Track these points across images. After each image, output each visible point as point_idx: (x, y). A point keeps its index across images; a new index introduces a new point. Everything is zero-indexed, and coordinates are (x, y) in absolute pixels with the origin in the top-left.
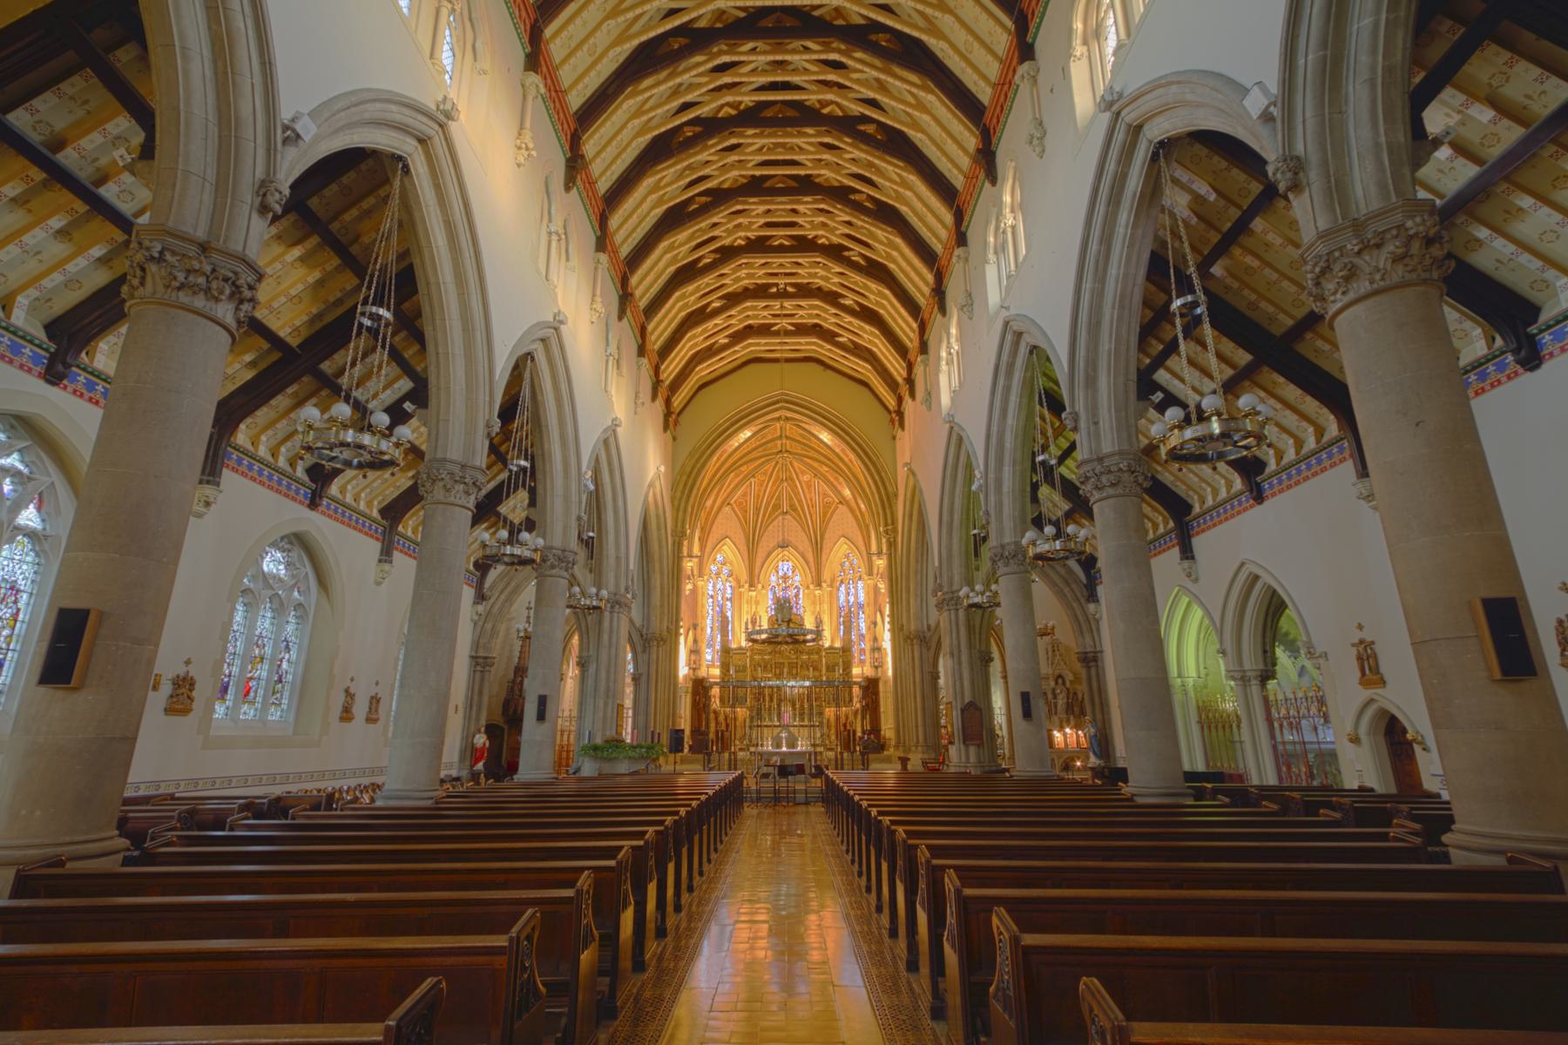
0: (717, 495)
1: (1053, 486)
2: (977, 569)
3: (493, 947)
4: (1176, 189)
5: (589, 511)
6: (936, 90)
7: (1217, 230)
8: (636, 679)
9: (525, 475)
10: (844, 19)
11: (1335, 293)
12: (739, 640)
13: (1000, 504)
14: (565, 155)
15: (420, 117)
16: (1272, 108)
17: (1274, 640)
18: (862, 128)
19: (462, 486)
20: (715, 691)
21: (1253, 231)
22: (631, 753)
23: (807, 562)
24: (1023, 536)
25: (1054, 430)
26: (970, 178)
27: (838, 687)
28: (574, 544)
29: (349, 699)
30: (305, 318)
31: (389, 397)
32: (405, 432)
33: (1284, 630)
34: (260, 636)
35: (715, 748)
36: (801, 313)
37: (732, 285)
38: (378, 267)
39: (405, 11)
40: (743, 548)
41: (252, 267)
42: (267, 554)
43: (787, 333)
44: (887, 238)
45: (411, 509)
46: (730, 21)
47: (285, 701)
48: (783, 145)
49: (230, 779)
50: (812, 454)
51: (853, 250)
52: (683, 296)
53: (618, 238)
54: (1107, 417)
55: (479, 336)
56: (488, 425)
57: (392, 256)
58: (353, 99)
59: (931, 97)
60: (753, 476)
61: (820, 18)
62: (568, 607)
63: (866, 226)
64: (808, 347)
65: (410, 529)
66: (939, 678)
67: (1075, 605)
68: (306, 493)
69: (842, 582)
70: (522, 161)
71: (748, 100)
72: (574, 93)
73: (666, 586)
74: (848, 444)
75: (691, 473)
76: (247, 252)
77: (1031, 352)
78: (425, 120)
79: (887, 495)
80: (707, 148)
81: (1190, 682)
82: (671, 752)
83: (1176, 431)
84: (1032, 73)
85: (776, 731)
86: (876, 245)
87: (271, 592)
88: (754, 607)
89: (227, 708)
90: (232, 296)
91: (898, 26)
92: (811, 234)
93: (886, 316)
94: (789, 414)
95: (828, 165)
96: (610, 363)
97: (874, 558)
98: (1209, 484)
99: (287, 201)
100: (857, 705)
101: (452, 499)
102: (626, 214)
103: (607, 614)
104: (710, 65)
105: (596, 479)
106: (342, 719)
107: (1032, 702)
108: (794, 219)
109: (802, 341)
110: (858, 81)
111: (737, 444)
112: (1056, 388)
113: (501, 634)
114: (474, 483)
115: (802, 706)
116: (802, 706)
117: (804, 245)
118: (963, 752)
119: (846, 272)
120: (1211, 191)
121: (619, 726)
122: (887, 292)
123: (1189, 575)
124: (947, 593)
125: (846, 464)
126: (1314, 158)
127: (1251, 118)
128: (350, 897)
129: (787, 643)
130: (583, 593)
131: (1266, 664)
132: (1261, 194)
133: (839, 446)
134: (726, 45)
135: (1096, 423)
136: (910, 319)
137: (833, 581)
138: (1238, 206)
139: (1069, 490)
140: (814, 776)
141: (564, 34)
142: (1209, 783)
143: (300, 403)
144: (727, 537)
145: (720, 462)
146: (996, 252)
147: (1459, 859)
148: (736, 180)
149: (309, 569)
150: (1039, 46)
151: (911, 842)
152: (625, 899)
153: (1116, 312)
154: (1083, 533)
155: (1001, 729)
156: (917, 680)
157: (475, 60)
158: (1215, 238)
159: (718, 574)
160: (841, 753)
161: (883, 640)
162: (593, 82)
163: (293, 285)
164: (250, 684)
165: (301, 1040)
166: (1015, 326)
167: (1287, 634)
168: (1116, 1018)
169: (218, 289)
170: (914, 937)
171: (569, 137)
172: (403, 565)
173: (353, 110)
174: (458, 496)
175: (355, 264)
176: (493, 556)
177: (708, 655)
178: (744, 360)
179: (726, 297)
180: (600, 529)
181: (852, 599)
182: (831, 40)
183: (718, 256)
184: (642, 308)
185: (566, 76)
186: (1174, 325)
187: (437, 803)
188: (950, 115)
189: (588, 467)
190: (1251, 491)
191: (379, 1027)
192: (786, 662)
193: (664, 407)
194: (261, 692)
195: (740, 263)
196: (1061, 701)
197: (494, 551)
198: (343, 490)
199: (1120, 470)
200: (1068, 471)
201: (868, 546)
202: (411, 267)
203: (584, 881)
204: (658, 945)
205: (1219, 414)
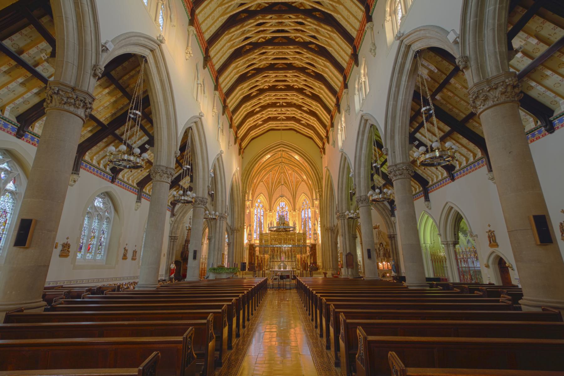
0: (258, 178)
1: (379, 175)
2: (352, 205)
4: (423, 68)
5: (212, 184)
7: (438, 83)
8: (229, 244)
9: (189, 171)
10: (304, 7)
11: (480, 105)
12: (266, 230)
14: (203, 56)
16: (457, 39)
18: (310, 46)
19: (166, 175)
20: (257, 249)
21: (451, 83)
22: (227, 271)
24: (368, 193)
26: (349, 64)
27: (301, 247)
28: (206, 196)
29: (125, 252)
30: (110, 114)
31: (140, 143)
32: (146, 155)
33: (462, 227)
34: (94, 229)
35: (257, 269)
36: (288, 112)
37: (263, 103)
38: (136, 96)
40: (267, 197)
42: (96, 199)
43: (283, 120)
46: (262, 8)
47: (102, 252)
48: (282, 52)
49: (83, 280)
50: (292, 163)
51: (307, 90)
52: (246, 107)
53: (222, 86)
54: (398, 150)
56: (176, 153)
57: (141, 92)
58: (127, 36)
59: (335, 35)
60: (271, 171)
61: (295, 7)
62: (204, 218)
64: (291, 125)
65: (147, 190)
66: (338, 244)
67: (386, 218)
69: (303, 209)
70: (188, 58)
71: (269, 36)
72: (207, 33)
73: (239, 211)
74: (305, 160)
76: (89, 91)
77: (371, 127)
78: (153, 43)
79: (319, 178)
80: (254, 53)
81: (428, 245)
82: (241, 270)
83: (423, 155)
84: (371, 26)
85: (279, 263)
87: (97, 213)
88: (271, 218)
89: (82, 255)
90: (83, 106)
91: (323, 10)
92: (292, 84)
93: (319, 114)
94: (284, 149)
95: (298, 59)
96: (220, 131)
97: (315, 201)
98: (430, 177)
99: (103, 73)
100: (308, 254)
102: (225, 77)
103: (218, 221)
104: (255, 24)
105: (215, 173)
108: (286, 79)
109: (288, 123)
110: (308, 29)
111: (265, 160)
112: (380, 140)
113: (180, 228)
114: (170, 174)
115: (289, 254)
116: (289, 254)
117: (289, 88)
118: (346, 271)
120: (436, 69)
121: (223, 261)
122: (319, 105)
123: (428, 207)
124: (341, 213)
125: (304, 167)
126: (473, 57)
127: (450, 42)
129: (283, 231)
130: (210, 214)
133: (302, 161)
134: (261, 16)
135: (394, 152)
136: (327, 115)
137: (300, 209)
138: (445, 74)
139: (384, 176)
140: (293, 279)
141: (203, 12)
142: (435, 282)
143: (108, 145)
144: (262, 193)
145: (259, 166)
146: (358, 91)
148: (265, 65)
149: (111, 205)
150: (374, 17)
151: (328, 303)
153: (401, 112)
154: (389, 192)
155: (360, 262)
157: (171, 22)
158: (437, 86)
159: (258, 207)
160: (303, 271)
161: (318, 230)
162: (213, 30)
164: (90, 246)
166: (365, 117)
167: (463, 228)
169: (78, 104)
171: (205, 49)
172: (145, 203)
173: (127, 39)
174: (165, 178)
175: (128, 95)
176: (178, 200)
177: (255, 236)
178: (268, 129)
181: (306, 216)
182: (299, 14)
183: (258, 92)
184: (231, 111)
185: (204, 27)
186: (422, 117)
187: (157, 289)
188: (342, 42)
189: (211, 168)
190: (450, 177)
192: (283, 238)
193: (239, 147)
194: (94, 249)
195: (266, 94)
197: (178, 198)
198: (123, 177)
199: (403, 169)
200: (384, 169)
201: (312, 196)
203: (210, 317)
204: (237, 340)
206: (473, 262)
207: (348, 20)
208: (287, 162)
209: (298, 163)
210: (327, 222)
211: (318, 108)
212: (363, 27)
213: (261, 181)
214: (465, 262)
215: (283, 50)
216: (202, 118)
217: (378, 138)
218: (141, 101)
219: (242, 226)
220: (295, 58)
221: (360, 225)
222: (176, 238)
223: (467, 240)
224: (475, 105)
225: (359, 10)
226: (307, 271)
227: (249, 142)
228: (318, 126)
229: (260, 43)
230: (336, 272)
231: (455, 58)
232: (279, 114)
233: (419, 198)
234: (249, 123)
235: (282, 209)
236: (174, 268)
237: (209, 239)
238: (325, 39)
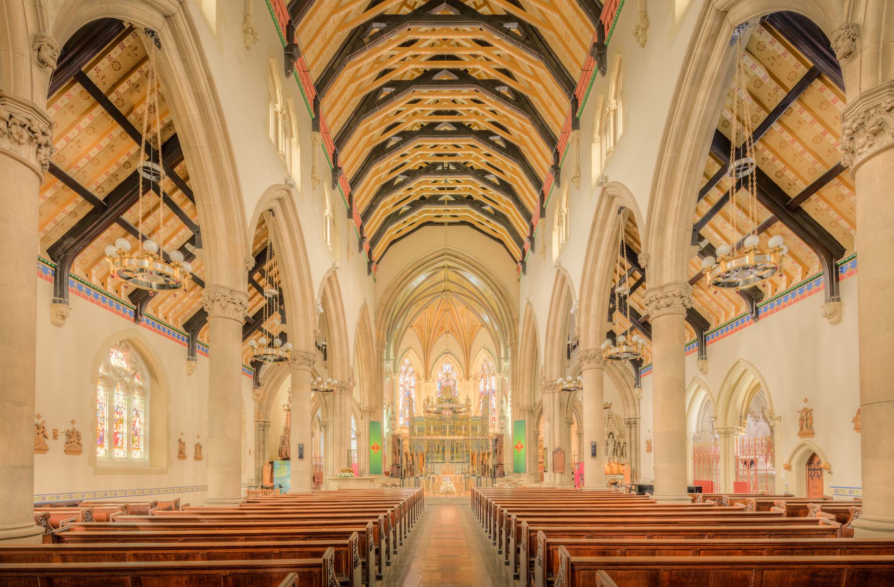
0: (405, 318)
11: (863, 146)
12: (419, 411)
14: (283, 44)
26: (565, 133)
28: (313, 349)
31: (176, 242)
40: (421, 355)
41: (41, 115)
42: (112, 353)
44: (521, 124)
49: (115, 492)
50: (465, 292)
52: (377, 172)
53: (329, 120)
60: (427, 308)
63: (507, 114)
65: (205, 339)
74: (489, 285)
75: (387, 304)
76: (35, 101)
77: (619, 212)
79: (513, 320)
86: (514, 130)
89: (106, 451)
90: (31, 139)
97: (503, 361)
98: (724, 310)
101: (227, 314)
102: (333, 101)
103: (337, 395)
105: (324, 303)
106: (179, 457)
109: (459, 209)
111: (416, 285)
114: (241, 303)
123: (702, 370)
126: (870, 26)
147: (859, 536)
153: (686, 175)
159: (406, 372)
166: (610, 191)
169: (17, 133)
174: (231, 312)
177: (401, 421)
179: (407, 173)
180: (330, 339)
189: (318, 297)
194: (125, 442)
201: (499, 353)
207: (566, 42)
208: (456, 291)
211: (516, 177)
213: (410, 325)
216: (292, 190)
222: (266, 424)
224: (851, 145)
228: (515, 216)
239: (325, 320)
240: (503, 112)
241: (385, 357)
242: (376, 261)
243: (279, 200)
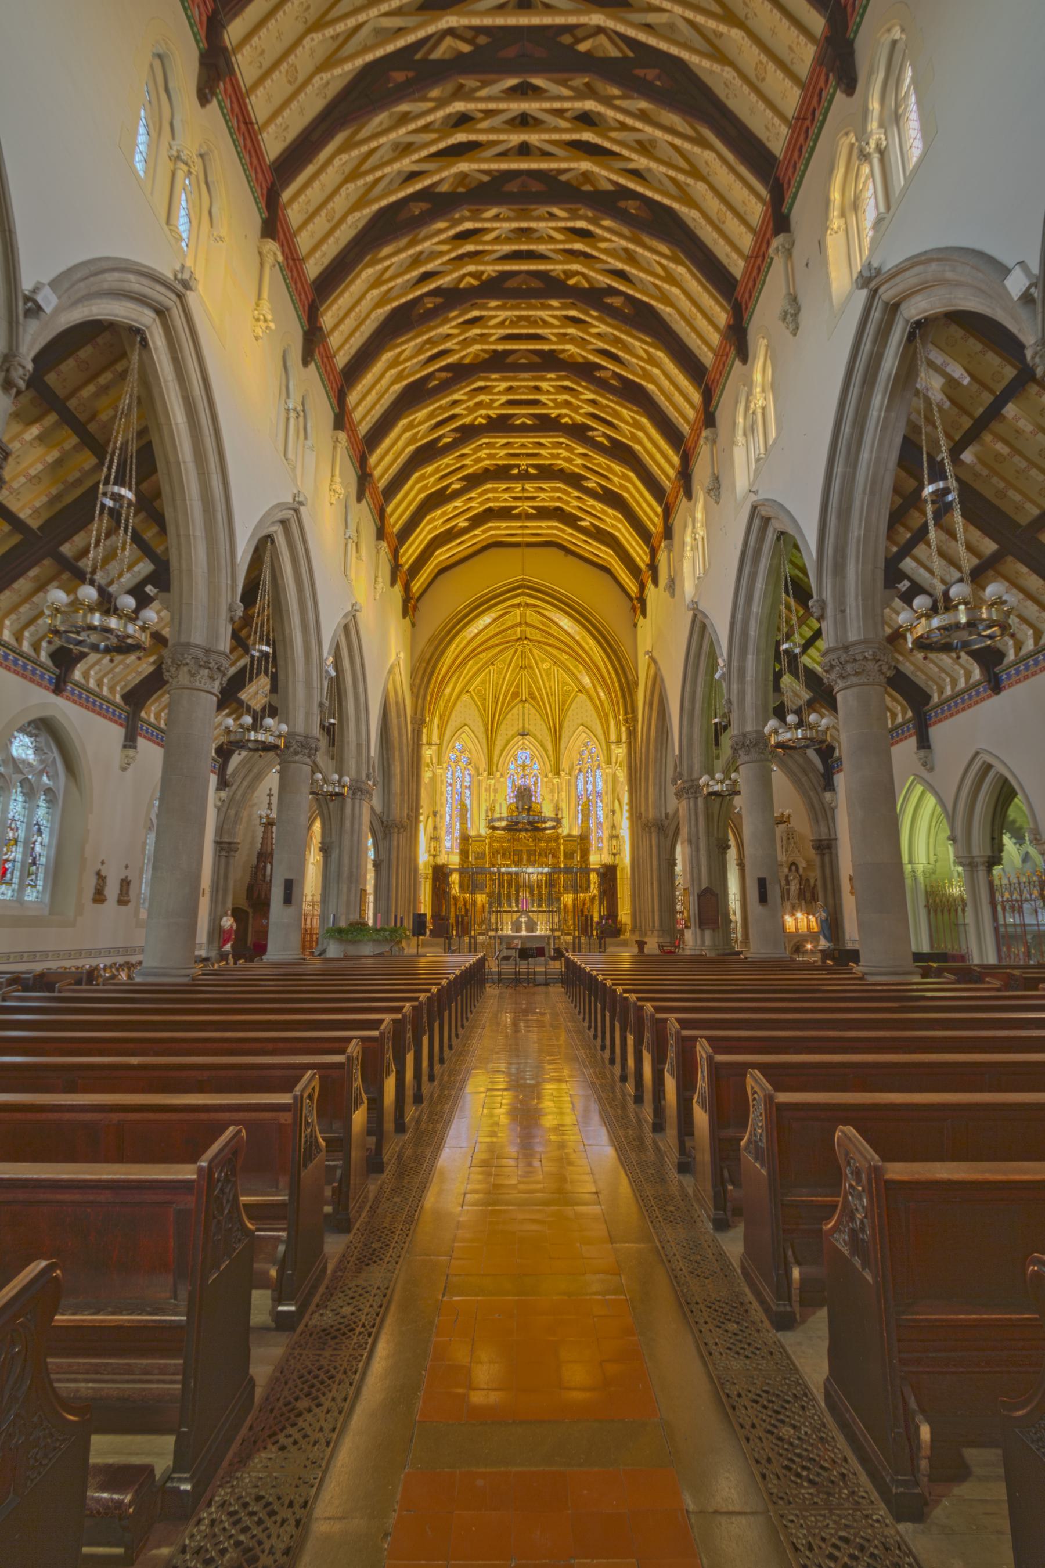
1: (797, 677)
2: (718, 758)
3: (278, 1104)
4: (931, 372)
5: (330, 698)
6: (687, 262)
7: (970, 415)
8: (377, 865)
9: (267, 662)
10: (593, 185)
12: (479, 828)
13: (742, 693)
14: (302, 327)
15: (159, 288)
16: (1033, 290)
17: (1002, 828)
18: (609, 300)
19: (207, 671)
20: (455, 878)
21: (1004, 417)
22: (375, 936)
23: (546, 751)
24: (766, 725)
25: (798, 618)
26: (720, 355)
27: (576, 874)
28: (316, 731)
29: (100, 881)
30: (45, 499)
31: (128, 579)
32: (151, 615)
33: (1011, 818)
34: (13, 820)
35: (454, 933)
36: (542, 495)
37: (472, 466)
38: (118, 445)
39: (142, 174)
42: (15, 738)
43: (529, 517)
45: (152, 695)
46: (473, 185)
47: (40, 883)
48: (527, 318)
50: (552, 641)
51: (596, 430)
52: (423, 478)
53: (357, 415)
54: (854, 604)
55: (220, 517)
56: (231, 609)
57: (132, 434)
58: (92, 269)
59: (681, 270)
60: (492, 664)
61: (567, 184)
62: (312, 793)
64: (549, 531)
66: (675, 865)
67: (811, 793)
68: (51, 679)
69: (580, 771)
70: (261, 334)
71: (490, 270)
72: (312, 261)
73: (406, 774)
77: (778, 538)
78: (163, 290)
79: (628, 683)
80: (447, 321)
81: (920, 868)
82: (414, 935)
83: (923, 620)
84: (787, 246)
85: (515, 916)
87: (22, 777)
88: (492, 794)
91: (649, 193)
92: (554, 413)
93: (630, 499)
94: (530, 601)
95: (573, 340)
96: (349, 545)
97: (613, 747)
98: (937, 683)
99: (30, 379)
100: (594, 890)
101: (197, 684)
103: (349, 801)
104: (452, 232)
105: (337, 665)
107: (768, 886)
108: (537, 397)
109: (543, 524)
110: (605, 251)
111: (476, 631)
112: (801, 575)
113: (245, 820)
114: (218, 668)
115: (540, 892)
116: (540, 892)
117: (546, 424)
119: (590, 453)
120: (965, 374)
121: (362, 911)
122: (631, 474)
123: (924, 764)
124: (686, 781)
127: (1011, 298)
128: (134, 1060)
129: (527, 830)
130: (325, 781)
131: (993, 851)
132: (1015, 379)
133: (579, 633)
134: (469, 211)
135: (843, 611)
136: (654, 503)
137: (571, 769)
138: (991, 391)
139: (812, 679)
140: (554, 959)
141: (302, 199)
142: (934, 962)
143: (41, 587)
144: (465, 725)
145: (459, 649)
146: (745, 434)
148: (476, 355)
149: (56, 754)
150: (795, 217)
151: (659, 1016)
152: (388, 1067)
154: (824, 722)
155: (735, 914)
156: (655, 867)
157: (212, 226)
158: (967, 423)
160: (579, 937)
161: (621, 828)
162: (331, 250)
163: (31, 466)
164: (7, 866)
165: (123, 1177)
166: (764, 511)
167: (1014, 822)
168: (873, 1159)
170: (660, 1102)
171: (306, 308)
172: (150, 754)
173: (92, 279)
175: (97, 446)
176: (237, 742)
178: (484, 544)
181: (590, 787)
182: (579, 206)
183: (458, 435)
184: (380, 489)
185: (304, 242)
186: (924, 514)
187: (193, 980)
188: (700, 289)
189: (329, 653)
190: (989, 681)
191: (192, 1167)
192: (525, 849)
193: (403, 593)
194: (17, 874)
195: (480, 442)
196: (794, 887)
197: (238, 737)
198: (86, 675)
199: (865, 659)
200: (812, 660)
202: (149, 445)
203: (354, 1049)
204: (416, 1110)
205: (966, 603)
206: (1036, 911)
209: (568, 640)
210: (647, 805)
212: (763, 249)
213: (465, 690)
214: (1013, 911)
215: (531, 313)
216: (302, 509)
217: (797, 572)
218: (134, 461)
219: (413, 814)
220: (565, 335)
221: (739, 815)
223: (1022, 853)
225: (752, 197)
226: (590, 937)
227: (430, 578)
228: (627, 535)
229: (464, 289)
230: (668, 940)
231: (1022, 347)
232: (515, 498)
233: (901, 740)
234: (431, 526)
235: (524, 770)
236: (232, 927)
237: (325, 849)
238: (652, 279)
239: (337, 686)
240: (605, 402)
241: (424, 741)
242: (417, 595)
243: (284, 523)
